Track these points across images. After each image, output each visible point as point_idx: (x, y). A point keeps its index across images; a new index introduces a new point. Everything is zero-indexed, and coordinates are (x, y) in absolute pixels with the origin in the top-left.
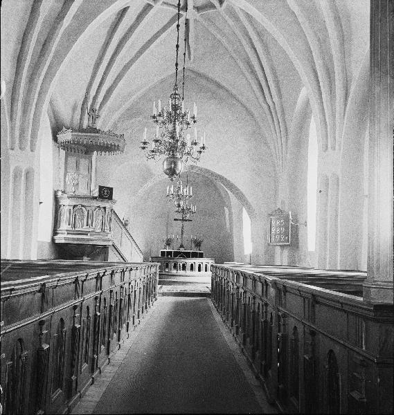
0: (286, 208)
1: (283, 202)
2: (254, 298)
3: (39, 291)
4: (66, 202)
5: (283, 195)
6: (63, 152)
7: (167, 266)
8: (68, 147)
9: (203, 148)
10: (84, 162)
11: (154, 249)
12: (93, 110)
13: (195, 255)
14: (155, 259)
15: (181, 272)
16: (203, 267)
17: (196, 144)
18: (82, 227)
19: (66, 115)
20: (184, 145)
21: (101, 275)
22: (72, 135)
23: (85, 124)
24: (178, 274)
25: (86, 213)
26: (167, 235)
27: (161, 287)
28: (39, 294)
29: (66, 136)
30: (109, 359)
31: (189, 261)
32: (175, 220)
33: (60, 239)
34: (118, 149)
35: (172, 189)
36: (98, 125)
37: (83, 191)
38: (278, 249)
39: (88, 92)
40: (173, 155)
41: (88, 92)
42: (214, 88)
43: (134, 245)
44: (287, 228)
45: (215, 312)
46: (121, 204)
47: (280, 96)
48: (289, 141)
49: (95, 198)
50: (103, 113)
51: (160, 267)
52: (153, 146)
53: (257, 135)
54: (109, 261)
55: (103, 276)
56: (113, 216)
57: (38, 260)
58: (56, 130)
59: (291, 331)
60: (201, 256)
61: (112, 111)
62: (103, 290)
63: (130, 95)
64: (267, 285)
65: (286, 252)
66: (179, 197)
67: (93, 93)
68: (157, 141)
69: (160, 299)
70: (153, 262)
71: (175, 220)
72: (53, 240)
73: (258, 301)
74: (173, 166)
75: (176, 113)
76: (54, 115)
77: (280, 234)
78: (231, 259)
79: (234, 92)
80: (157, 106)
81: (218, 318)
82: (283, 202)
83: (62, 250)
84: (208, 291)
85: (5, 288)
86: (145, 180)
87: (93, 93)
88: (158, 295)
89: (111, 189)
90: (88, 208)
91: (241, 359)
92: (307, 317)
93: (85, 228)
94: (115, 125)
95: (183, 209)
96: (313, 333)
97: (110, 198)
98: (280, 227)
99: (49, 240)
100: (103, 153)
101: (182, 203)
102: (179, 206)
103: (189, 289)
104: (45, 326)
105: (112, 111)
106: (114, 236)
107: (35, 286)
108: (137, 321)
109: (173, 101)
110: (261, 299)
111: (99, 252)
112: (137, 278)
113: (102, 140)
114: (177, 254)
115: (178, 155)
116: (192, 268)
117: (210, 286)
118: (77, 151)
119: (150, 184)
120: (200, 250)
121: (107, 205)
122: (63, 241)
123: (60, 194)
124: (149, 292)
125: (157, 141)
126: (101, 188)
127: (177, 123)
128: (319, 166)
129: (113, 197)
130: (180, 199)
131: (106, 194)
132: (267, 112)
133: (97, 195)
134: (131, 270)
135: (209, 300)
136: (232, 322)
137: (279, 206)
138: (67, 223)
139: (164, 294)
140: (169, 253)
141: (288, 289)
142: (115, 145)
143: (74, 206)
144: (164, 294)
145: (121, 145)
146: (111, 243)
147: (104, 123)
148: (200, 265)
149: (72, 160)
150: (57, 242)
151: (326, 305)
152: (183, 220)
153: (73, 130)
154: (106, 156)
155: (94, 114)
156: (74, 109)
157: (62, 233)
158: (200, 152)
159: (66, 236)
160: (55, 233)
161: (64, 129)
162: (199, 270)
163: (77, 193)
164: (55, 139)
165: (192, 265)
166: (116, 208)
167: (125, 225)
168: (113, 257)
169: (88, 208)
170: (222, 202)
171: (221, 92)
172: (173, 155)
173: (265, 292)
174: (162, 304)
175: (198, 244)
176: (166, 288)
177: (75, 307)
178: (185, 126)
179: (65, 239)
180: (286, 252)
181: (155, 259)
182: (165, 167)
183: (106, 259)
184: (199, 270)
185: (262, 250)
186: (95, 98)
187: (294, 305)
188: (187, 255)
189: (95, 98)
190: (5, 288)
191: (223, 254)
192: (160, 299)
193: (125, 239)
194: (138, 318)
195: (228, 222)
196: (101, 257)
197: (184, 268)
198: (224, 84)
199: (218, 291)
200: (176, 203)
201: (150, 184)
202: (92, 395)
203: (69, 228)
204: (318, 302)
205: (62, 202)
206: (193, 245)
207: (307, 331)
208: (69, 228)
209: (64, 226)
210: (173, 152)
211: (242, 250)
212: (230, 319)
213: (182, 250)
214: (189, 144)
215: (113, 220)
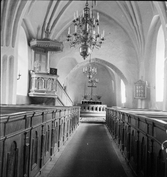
0: (144, 80)
1: (142, 77)
2: (120, 120)
3: (24, 119)
4: (34, 76)
5: (142, 74)
6: (33, 51)
7: (85, 108)
8: (36, 49)
9: (103, 39)
10: (44, 57)
11: (79, 100)
12: (47, 30)
13: (98, 103)
14: (79, 105)
15: (91, 111)
16: (102, 109)
17: (98, 36)
18: (42, 88)
19: (34, 32)
20: (91, 38)
21: (55, 111)
22: (37, 42)
23: (44, 37)
24: (90, 112)
25: (44, 81)
26: (85, 94)
27: (81, 119)
28: (24, 120)
29: (34, 43)
30: (40, 171)
31: (95, 106)
32: (88, 86)
33: (32, 94)
34: (60, 50)
35: (86, 69)
36: (51, 37)
37: (43, 71)
38: (139, 101)
39: (45, 22)
40: (85, 43)
41: (45, 22)
42: (107, 19)
43: (68, 98)
44: (144, 90)
45: (108, 133)
46: (62, 78)
47: (141, 22)
48: (145, 48)
49: (48, 74)
50: (53, 31)
51: (81, 109)
52: (74, 38)
53: (129, 43)
54: (56, 105)
55: (56, 112)
56: (58, 83)
57: (17, 105)
58: (29, 41)
59: (141, 140)
60: (100, 103)
61: (57, 31)
62: (56, 118)
63: (66, 23)
64: (124, 115)
65: (144, 102)
66: (90, 73)
67: (47, 21)
68: (75, 35)
69: (80, 124)
70: (78, 106)
71: (88, 86)
72: (28, 95)
73: (121, 121)
74: (85, 50)
75: (87, 19)
76: (29, 33)
77: (141, 93)
78: (115, 105)
79: (118, 21)
80: (76, 15)
81: (110, 137)
82: (142, 77)
83: (33, 100)
84: (104, 121)
85: (3, 118)
86: (73, 66)
87: (47, 21)
88: (79, 122)
89: (56, 70)
90: (45, 79)
91: (126, 168)
92: (137, 126)
93: (44, 89)
94: (59, 38)
95: (92, 81)
96: (152, 141)
97: (56, 74)
98: (141, 89)
99: (26, 95)
100: (51, 52)
101: (91, 76)
102: (90, 78)
103: (95, 119)
104: (27, 135)
105: (57, 31)
106: (58, 94)
107: (31, 114)
108: (65, 139)
109: (86, 12)
110: (127, 124)
111: (51, 101)
112: (66, 116)
113: (52, 45)
114: (89, 103)
115: (88, 44)
116: (96, 109)
117: (105, 118)
118: (40, 51)
119: (75, 68)
120: (100, 101)
121: (54, 77)
122: (33, 96)
123: (31, 72)
124: (74, 121)
125: (75, 35)
126: (51, 69)
127: (88, 25)
128: (124, 82)
129: (57, 74)
130: (90, 74)
131: (54, 72)
132: (134, 31)
133: (49, 72)
134: (60, 111)
135: (105, 125)
136: (114, 133)
137: (140, 79)
138: (35, 86)
139: (82, 122)
140: (86, 102)
141: (140, 119)
142: (58, 47)
143: (38, 78)
144: (82, 122)
145: (61, 48)
146: (56, 97)
147: (53, 36)
148: (100, 108)
149: (38, 55)
150: (30, 96)
151: (158, 128)
152: (92, 87)
153: (38, 40)
154: (57, 54)
155: (48, 33)
156: (38, 29)
157: (33, 92)
158: (101, 43)
159: (34, 93)
160: (29, 92)
161: (33, 39)
162: (100, 110)
163: (40, 72)
164: (29, 44)
165: (96, 108)
166: (59, 79)
167: (65, 89)
168: (57, 103)
169: (45, 79)
170: (110, 77)
171: (110, 21)
172: (85, 43)
173: (123, 118)
174: (81, 127)
175: (99, 98)
176: (84, 119)
177: (25, 133)
178: (93, 28)
179: (34, 94)
180: (144, 102)
181: (79, 105)
182: (81, 51)
183: (54, 104)
184: (100, 110)
185: (131, 100)
186: (49, 24)
187: (10, 5)
188: (94, 103)
189: (49, 24)
190: (3, 118)
191: (111, 103)
192: (80, 124)
193: (64, 95)
194: (67, 136)
195: (113, 89)
196: (52, 103)
197: (92, 109)
198: (113, 17)
199: (110, 121)
200: (88, 76)
201: (75, 68)
202: (49, 165)
203: (36, 89)
204: (155, 126)
205: (32, 76)
206: (97, 99)
207: (137, 131)
208: (36, 89)
209: (33, 88)
210: (85, 42)
211: (120, 101)
212: (110, 127)
213: (91, 101)
214: (94, 38)
215: (57, 84)
